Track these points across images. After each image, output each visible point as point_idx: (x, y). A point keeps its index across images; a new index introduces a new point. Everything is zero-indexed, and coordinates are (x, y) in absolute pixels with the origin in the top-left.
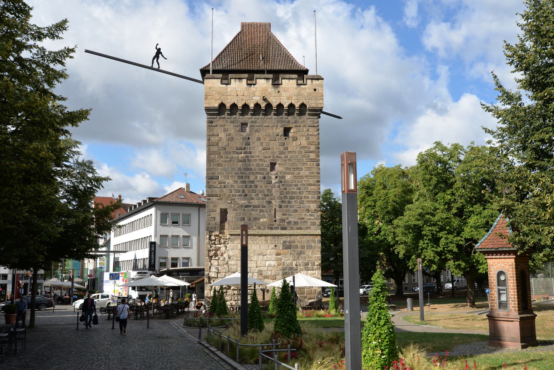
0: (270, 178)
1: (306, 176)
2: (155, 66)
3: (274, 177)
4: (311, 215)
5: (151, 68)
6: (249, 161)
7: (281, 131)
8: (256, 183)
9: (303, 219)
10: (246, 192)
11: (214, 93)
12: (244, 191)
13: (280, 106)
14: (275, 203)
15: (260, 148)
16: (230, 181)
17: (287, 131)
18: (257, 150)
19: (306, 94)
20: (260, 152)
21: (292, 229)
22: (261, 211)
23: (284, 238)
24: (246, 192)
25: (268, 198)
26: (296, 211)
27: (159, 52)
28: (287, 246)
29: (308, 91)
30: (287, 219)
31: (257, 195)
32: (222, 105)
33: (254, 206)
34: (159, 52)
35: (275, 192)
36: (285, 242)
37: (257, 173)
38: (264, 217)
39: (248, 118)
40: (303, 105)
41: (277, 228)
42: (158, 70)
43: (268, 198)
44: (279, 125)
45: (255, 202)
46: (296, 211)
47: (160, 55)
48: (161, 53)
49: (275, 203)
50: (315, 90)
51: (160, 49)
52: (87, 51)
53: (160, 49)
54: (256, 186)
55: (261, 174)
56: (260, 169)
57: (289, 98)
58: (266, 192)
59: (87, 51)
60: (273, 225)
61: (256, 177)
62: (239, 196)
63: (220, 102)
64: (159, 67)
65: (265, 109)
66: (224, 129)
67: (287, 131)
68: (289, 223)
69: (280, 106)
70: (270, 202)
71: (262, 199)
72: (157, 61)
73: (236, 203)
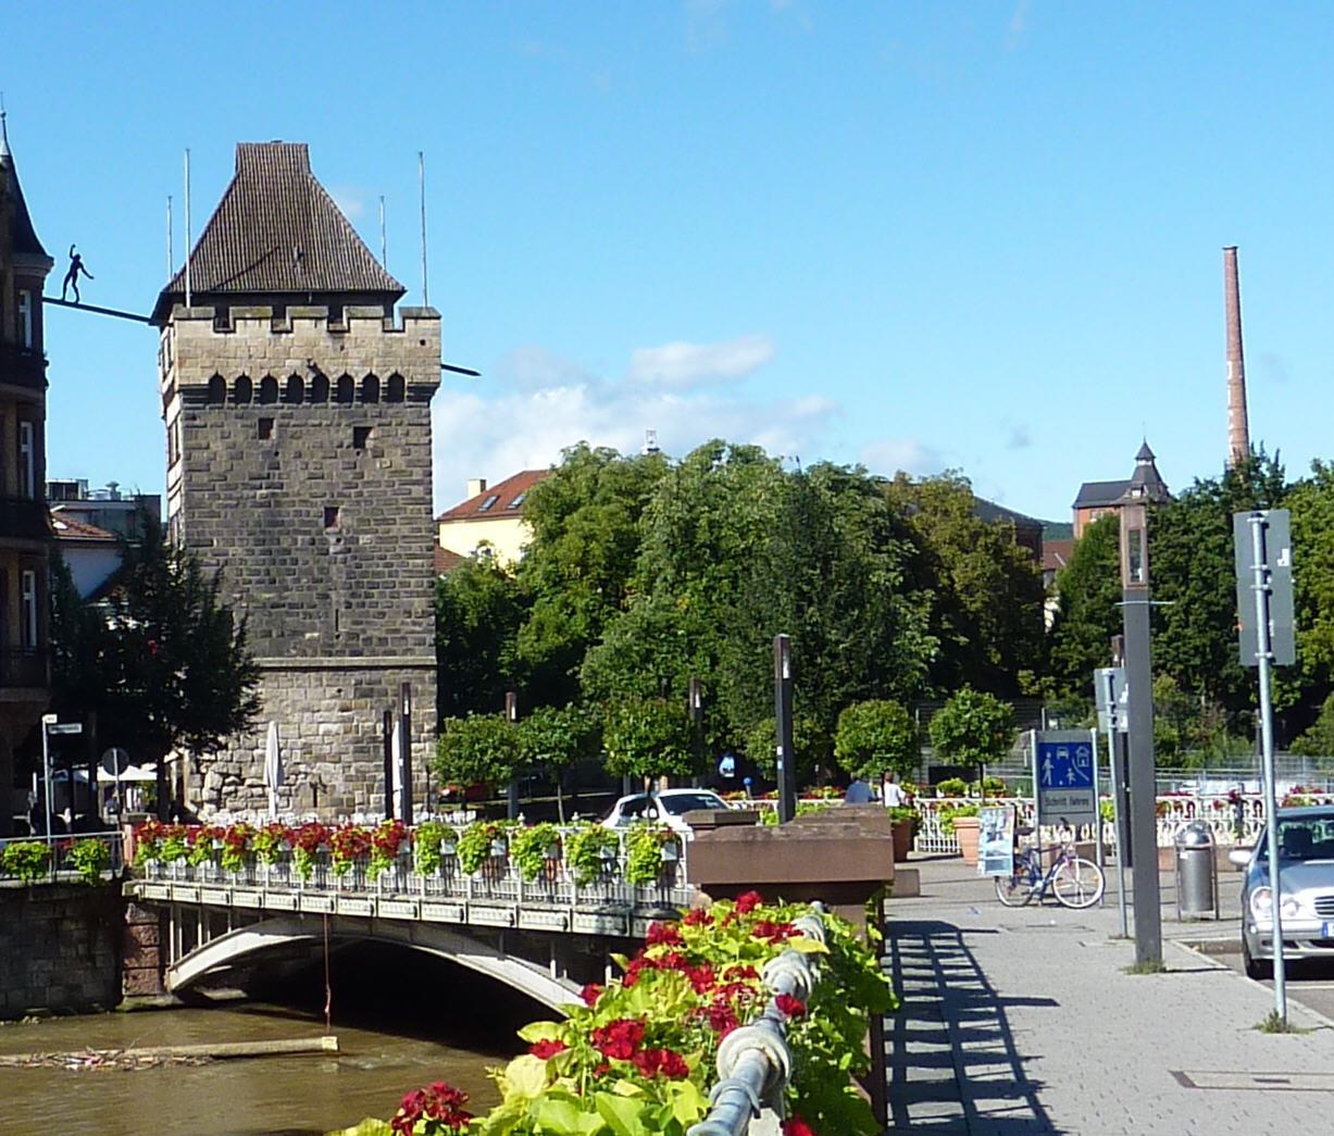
0: (325, 542)
2: (70, 298)
5: (62, 302)
7: (347, 435)
9: (397, 631)
12: (268, 572)
13: (346, 379)
17: (360, 435)
18: (295, 479)
21: (374, 653)
23: (357, 675)
25: (320, 587)
29: (407, 345)
30: (364, 631)
31: (298, 580)
32: (217, 380)
33: (292, 606)
35: (337, 573)
40: (396, 379)
41: (341, 653)
42: (76, 305)
43: (320, 587)
45: (294, 596)
46: (383, 614)
50: (423, 343)
54: (295, 562)
55: (305, 533)
56: (303, 523)
57: (364, 363)
61: (295, 542)
65: (313, 389)
67: (360, 435)
68: (368, 640)
69: (346, 379)
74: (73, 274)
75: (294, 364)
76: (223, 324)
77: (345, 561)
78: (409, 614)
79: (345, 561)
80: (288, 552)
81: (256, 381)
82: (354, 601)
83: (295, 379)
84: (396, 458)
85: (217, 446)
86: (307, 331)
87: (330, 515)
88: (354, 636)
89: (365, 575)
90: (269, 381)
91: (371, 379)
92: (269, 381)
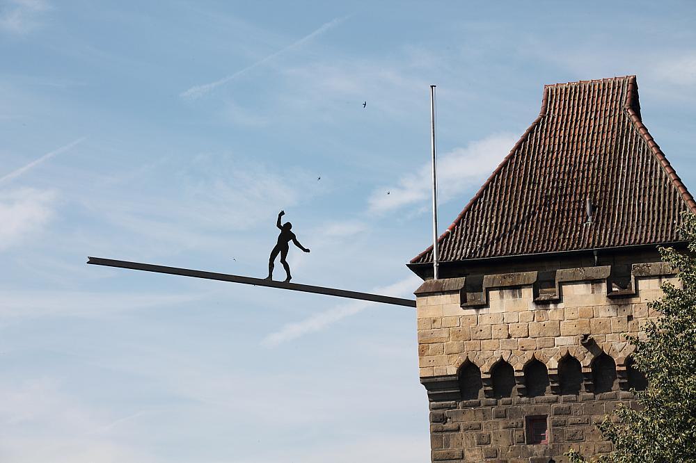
2: (279, 275)
5: (268, 282)
11: (445, 335)
27: (286, 234)
32: (468, 368)
34: (286, 234)
39: (547, 402)
42: (287, 285)
47: (291, 243)
48: (293, 237)
51: (288, 225)
52: (93, 261)
53: (288, 225)
59: (93, 261)
63: (460, 359)
64: (289, 277)
66: (480, 437)
72: (283, 261)
74: (281, 248)
75: (567, 343)
81: (518, 366)
83: (568, 362)
86: (582, 298)
90: (535, 366)
92: (535, 366)
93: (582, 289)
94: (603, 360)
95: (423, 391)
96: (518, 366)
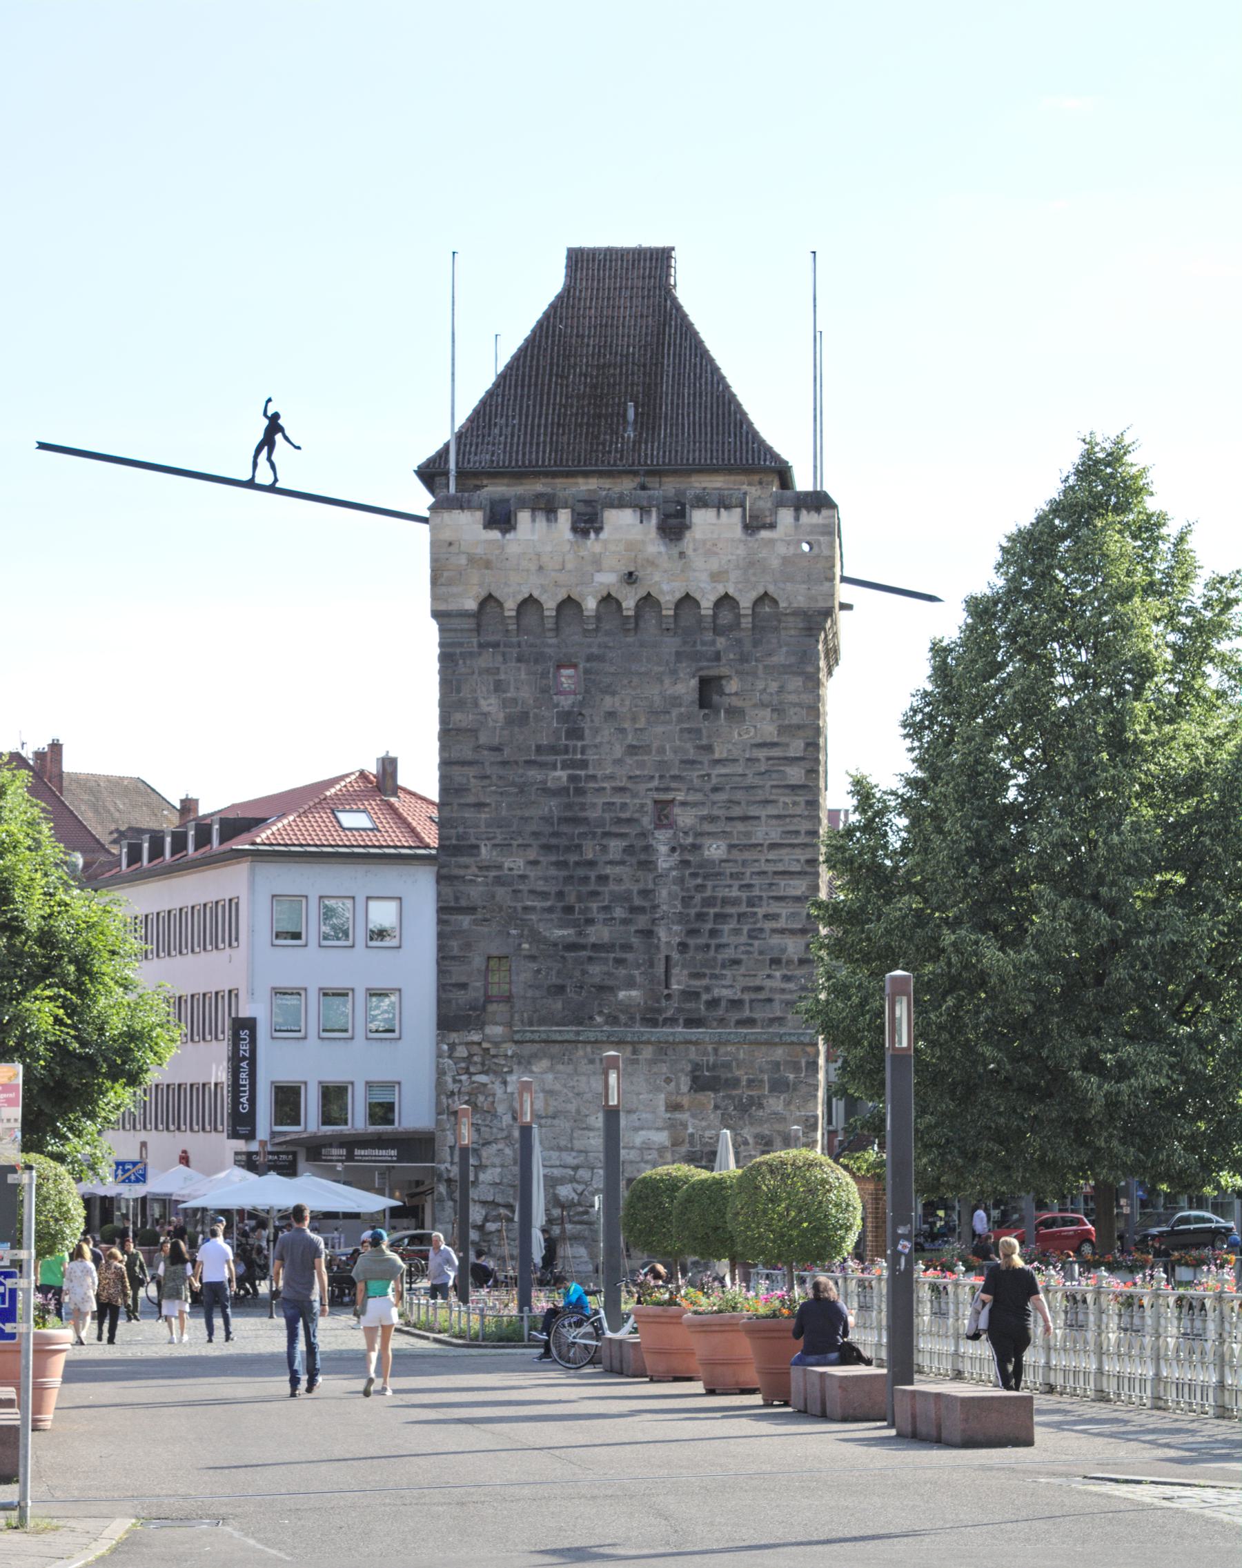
1: (773, 846)
2: (264, 477)
3: (663, 849)
4: (786, 978)
5: (251, 484)
6: (580, 792)
7: (687, 687)
8: (608, 870)
9: (759, 989)
10: (571, 899)
12: (560, 895)
13: (687, 600)
14: (668, 936)
15: (618, 751)
16: (515, 863)
17: (708, 689)
18: (606, 752)
19: (775, 563)
20: (618, 762)
22: (619, 962)
24: (571, 899)
25: (642, 921)
26: (736, 962)
27: (274, 426)
28: (700, 1084)
30: (708, 989)
33: (595, 947)
34: (274, 426)
36: (697, 1067)
37: (606, 834)
38: (630, 984)
41: (672, 1021)
42: (272, 489)
43: (642, 921)
44: (685, 668)
45: (599, 933)
49: (668, 936)
52: (43, 446)
54: (603, 879)
57: (716, 577)
58: (638, 902)
59: (43, 446)
60: (659, 1011)
61: (604, 848)
62: (550, 910)
65: (630, 619)
68: (713, 1003)
69: (687, 600)
70: (648, 934)
71: (625, 922)
73: (535, 937)
74: (268, 442)
75: (607, 579)
76: (501, 519)
77: (681, 881)
78: (775, 962)
79: (681, 881)
80: (591, 864)
81: (550, 605)
82: (691, 942)
83: (608, 600)
84: (768, 729)
85: (490, 705)
87: (663, 811)
88: (690, 995)
89: (709, 902)
90: (569, 604)
91: (726, 600)
92: (569, 604)
93: (626, 517)
94: (648, 600)
95: (433, 626)
96: (550, 605)
